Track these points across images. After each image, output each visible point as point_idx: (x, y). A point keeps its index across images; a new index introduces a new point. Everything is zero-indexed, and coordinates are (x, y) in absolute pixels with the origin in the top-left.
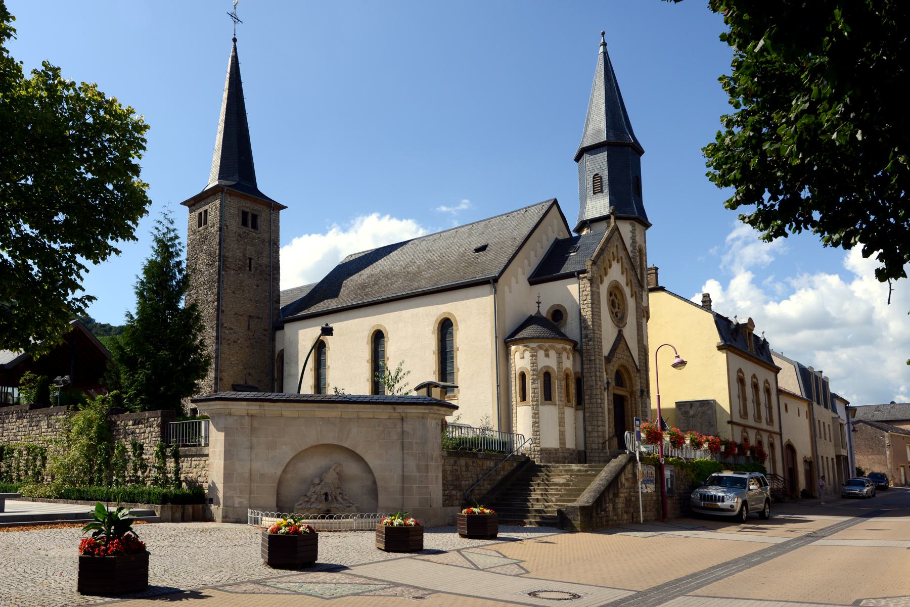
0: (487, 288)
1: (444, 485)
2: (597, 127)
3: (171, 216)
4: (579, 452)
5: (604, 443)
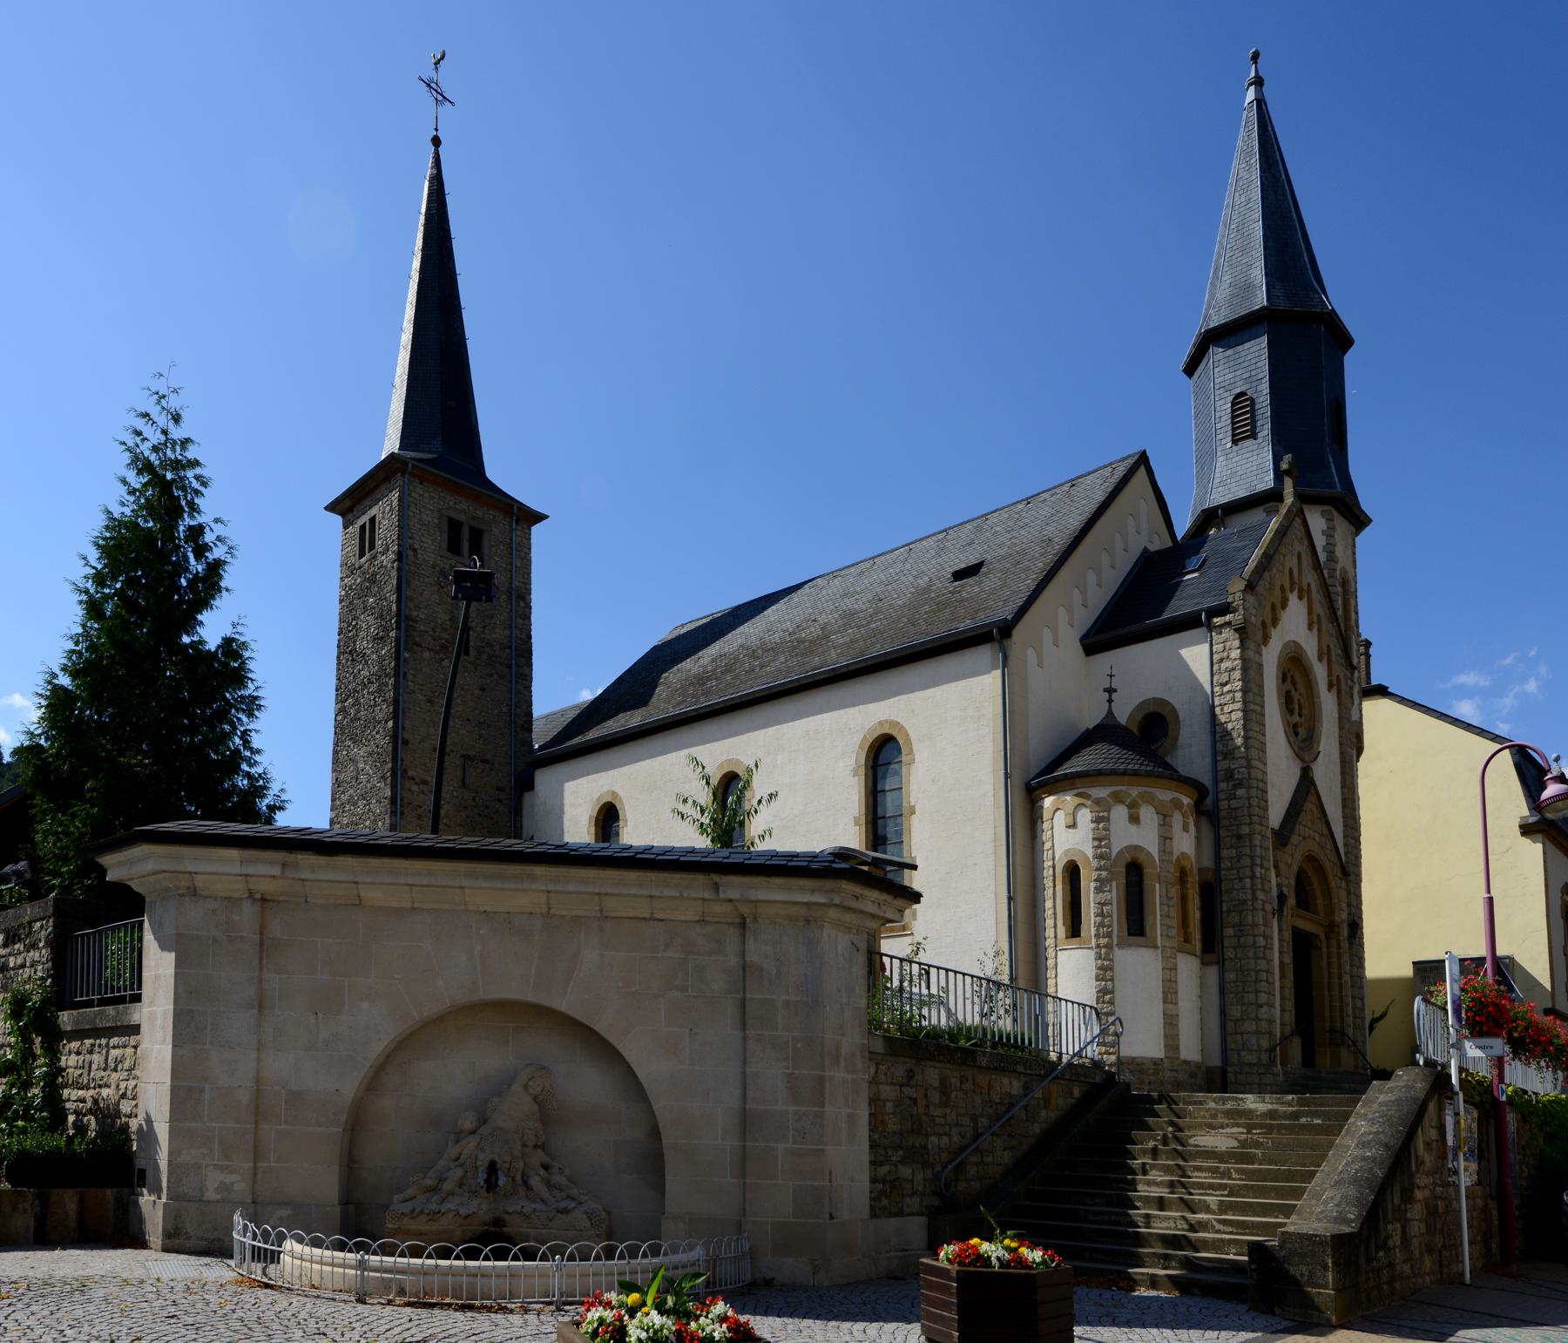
0: (984, 653)
1: (873, 1145)
2: (1238, 275)
3: (174, 402)
4: (1210, 1072)
5: (1272, 1050)
